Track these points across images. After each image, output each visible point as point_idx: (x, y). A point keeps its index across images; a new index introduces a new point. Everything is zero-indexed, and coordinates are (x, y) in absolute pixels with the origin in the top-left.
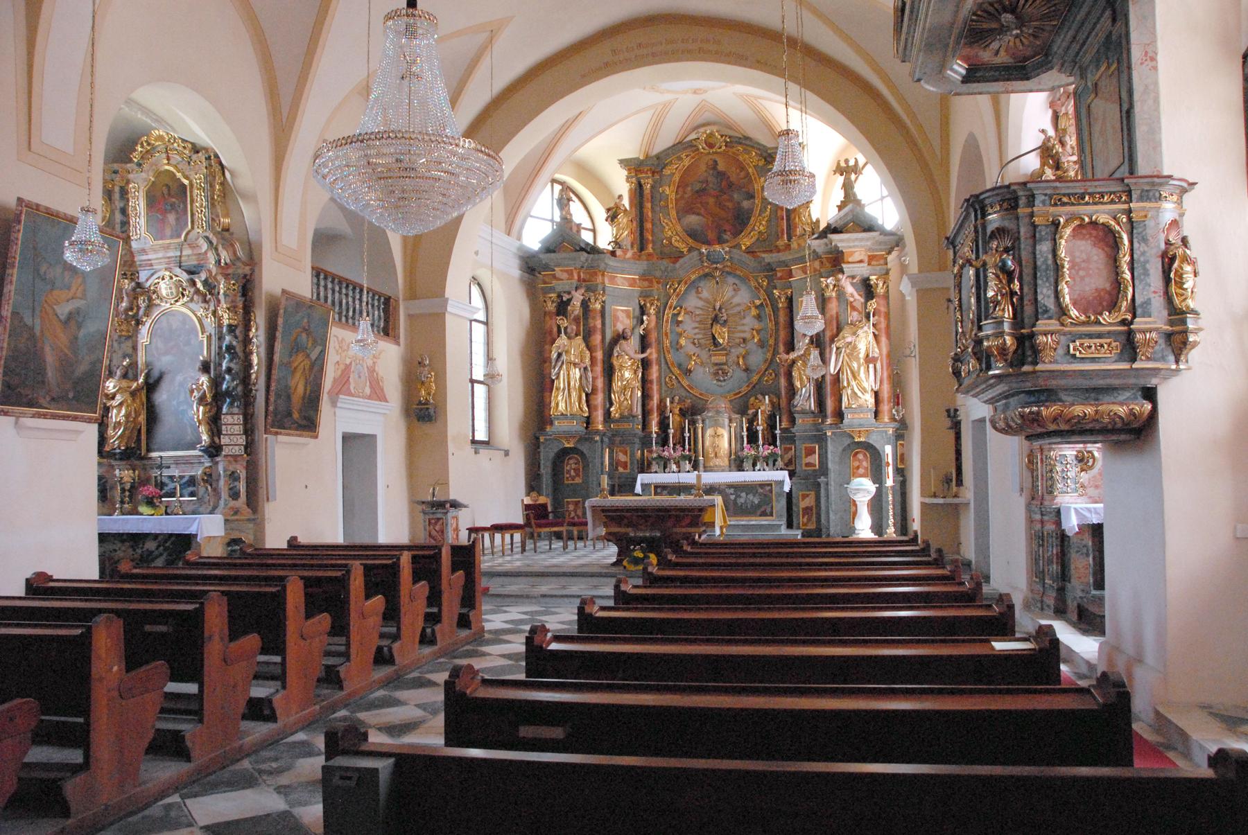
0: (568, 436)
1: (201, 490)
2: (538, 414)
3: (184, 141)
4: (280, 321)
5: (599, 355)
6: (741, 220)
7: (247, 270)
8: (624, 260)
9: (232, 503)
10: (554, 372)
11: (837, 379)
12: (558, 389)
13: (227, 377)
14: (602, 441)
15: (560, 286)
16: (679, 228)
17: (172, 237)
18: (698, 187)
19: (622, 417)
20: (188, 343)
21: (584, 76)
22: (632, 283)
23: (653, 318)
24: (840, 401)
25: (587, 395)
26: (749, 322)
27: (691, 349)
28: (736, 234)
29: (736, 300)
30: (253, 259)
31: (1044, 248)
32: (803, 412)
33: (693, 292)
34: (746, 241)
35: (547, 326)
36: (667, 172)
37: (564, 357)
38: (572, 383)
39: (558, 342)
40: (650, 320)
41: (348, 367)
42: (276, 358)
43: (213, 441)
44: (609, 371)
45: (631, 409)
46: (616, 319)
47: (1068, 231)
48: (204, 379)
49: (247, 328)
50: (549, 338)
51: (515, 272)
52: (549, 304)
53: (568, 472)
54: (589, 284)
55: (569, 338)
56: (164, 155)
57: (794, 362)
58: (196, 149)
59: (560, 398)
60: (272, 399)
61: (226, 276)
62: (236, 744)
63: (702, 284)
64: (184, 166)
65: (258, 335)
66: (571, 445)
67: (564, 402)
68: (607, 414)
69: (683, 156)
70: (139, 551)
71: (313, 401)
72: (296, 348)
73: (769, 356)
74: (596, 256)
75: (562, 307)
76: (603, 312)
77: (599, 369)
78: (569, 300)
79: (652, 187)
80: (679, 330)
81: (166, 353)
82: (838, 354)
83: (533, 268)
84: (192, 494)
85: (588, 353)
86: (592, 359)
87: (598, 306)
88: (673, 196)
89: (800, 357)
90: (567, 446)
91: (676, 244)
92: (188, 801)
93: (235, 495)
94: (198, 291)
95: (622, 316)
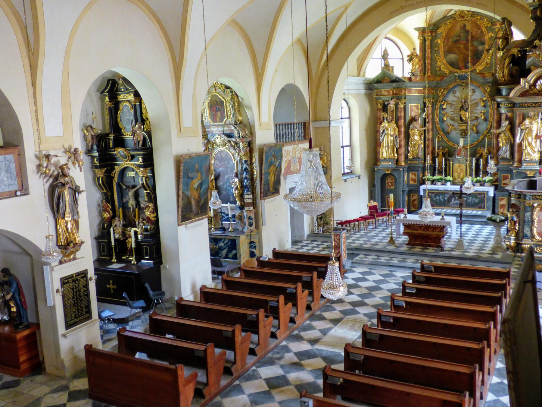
0: (387, 169)
1: (237, 221)
2: (373, 158)
3: (221, 84)
4: (264, 157)
5: (403, 129)
6: (477, 56)
7: (250, 139)
8: (417, 82)
9: (250, 228)
10: (381, 138)
11: (520, 145)
12: (383, 146)
13: (246, 180)
14: (404, 171)
15: (383, 98)
16: (445, 62)
17: (219, 122)
18: (455, 39)
19: (413, 158)
20: (229, 163)
21: (391, 13)
22: (420, 92)
23: (430, 108)
24: (522, 155)
25: (397, 149)
26: (480, 108)
27: (450, 122)
28: (474, 64)
29: (474, 97)
30: (252, 133)
31: (528, 214)
32: (503, 159)
33: (452, 92)
34: (479, 68)
35: (378, 116)
36: (439, 31)
37: (386, 132)
38: (389, 144)
39: (383, 124)
40: (429, 110)
41: (290, 161)
42: (263, 172)
43: (241, 204)
44: (408, 137)
45: (418, 154)
46: (411, 110)
47: (538, 209)
48: (237, 180)
49: (251, 159)
50: (379, 121)
51: (362, 91)
52: (379, 105)
53: (388, 183)
54: (397, 97)
55: (388, 122)
56: (214, 89)
57: (500, 133)
58: (227, 87)
59: (384, 150)
60: (263, 187)
61: (243, 142)
62: (267, 349)
63: (456, 89)
64: (222, 93)
65: (256, 164)
66: (389, 172)
67: (384, 153)
68: (406, 157)
69: (448, 23)
70: (218, 246)
71: (277, 182)
72: (271, 164)
73: (489, 127)
74: (401, 83)
75: (385, 108)
76: (405, 108)
77: (402, 136)
78: (388, 104)
79: (431, 41)
80: (443, 112)
81: (221, 167)
82: (521, 132)
83: (371, 87)
84: (234, 221)
85: (397, 130)
86: (400, 132)
87: (402, 106)
88: (442, 44)
89: (503, 132)
90: (387, 172)
91: (443, 70)
92: (258, 369)
93: (251, 225)
94: (232, 145)
95: (414, 109)
